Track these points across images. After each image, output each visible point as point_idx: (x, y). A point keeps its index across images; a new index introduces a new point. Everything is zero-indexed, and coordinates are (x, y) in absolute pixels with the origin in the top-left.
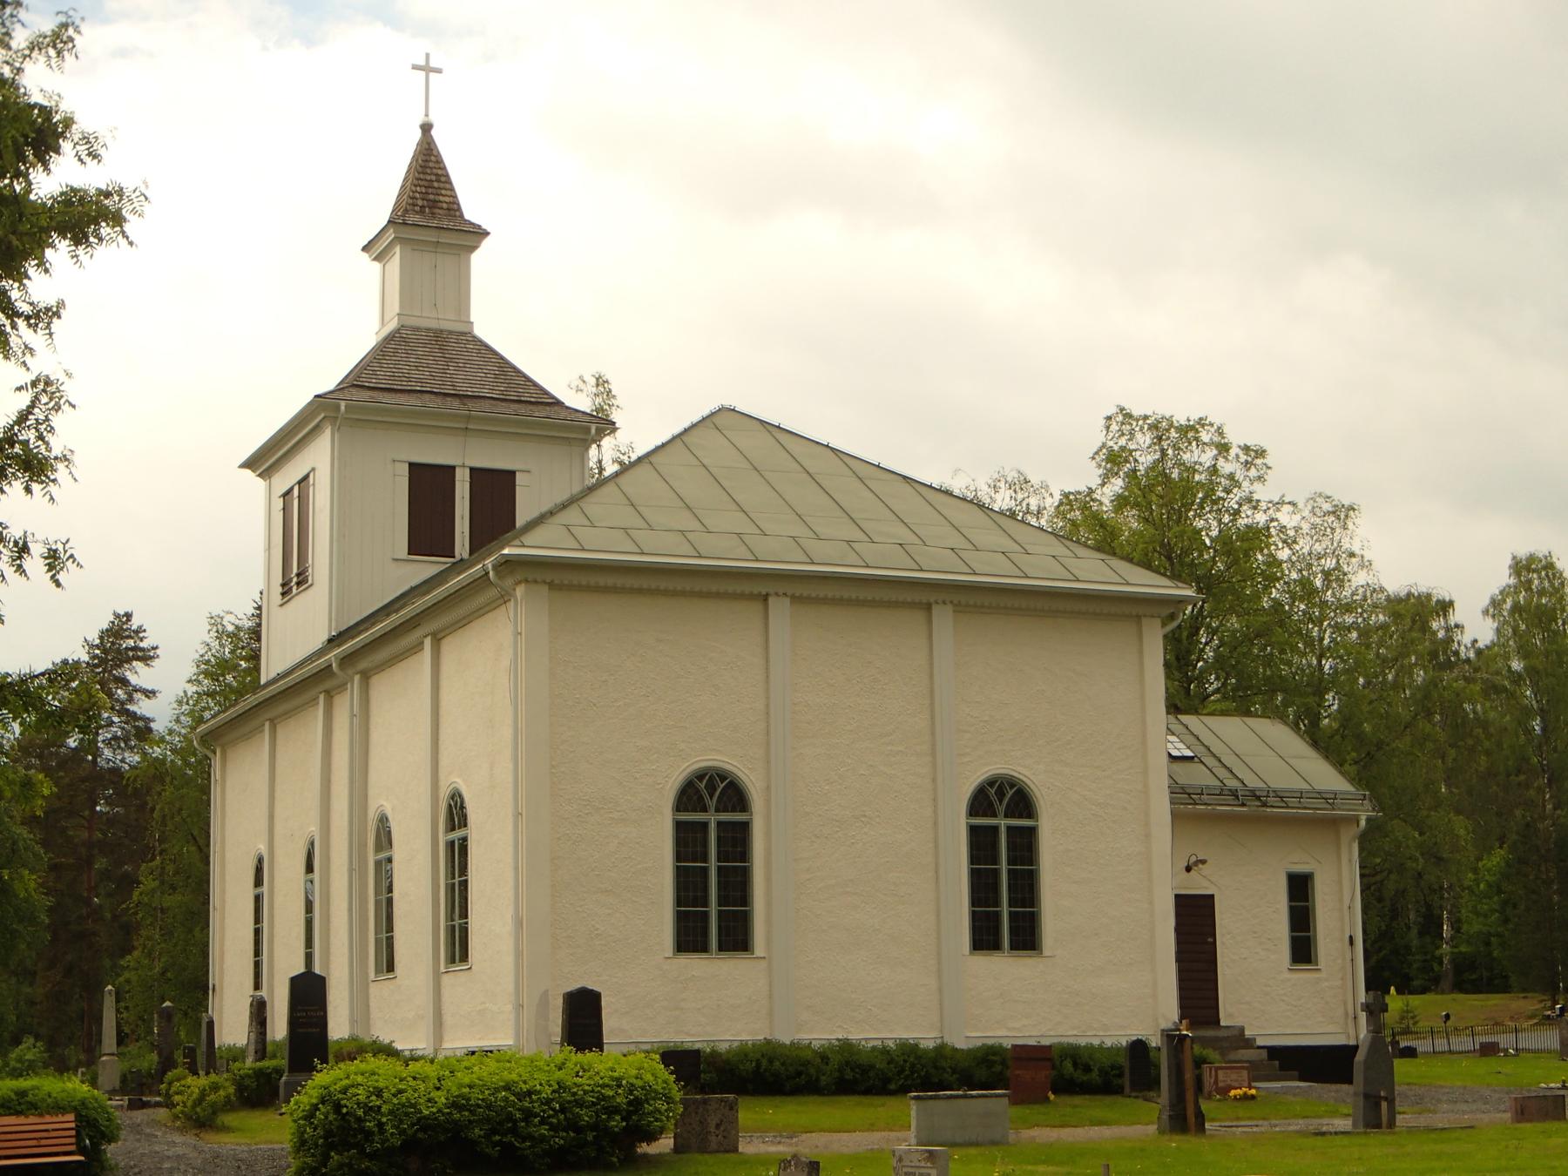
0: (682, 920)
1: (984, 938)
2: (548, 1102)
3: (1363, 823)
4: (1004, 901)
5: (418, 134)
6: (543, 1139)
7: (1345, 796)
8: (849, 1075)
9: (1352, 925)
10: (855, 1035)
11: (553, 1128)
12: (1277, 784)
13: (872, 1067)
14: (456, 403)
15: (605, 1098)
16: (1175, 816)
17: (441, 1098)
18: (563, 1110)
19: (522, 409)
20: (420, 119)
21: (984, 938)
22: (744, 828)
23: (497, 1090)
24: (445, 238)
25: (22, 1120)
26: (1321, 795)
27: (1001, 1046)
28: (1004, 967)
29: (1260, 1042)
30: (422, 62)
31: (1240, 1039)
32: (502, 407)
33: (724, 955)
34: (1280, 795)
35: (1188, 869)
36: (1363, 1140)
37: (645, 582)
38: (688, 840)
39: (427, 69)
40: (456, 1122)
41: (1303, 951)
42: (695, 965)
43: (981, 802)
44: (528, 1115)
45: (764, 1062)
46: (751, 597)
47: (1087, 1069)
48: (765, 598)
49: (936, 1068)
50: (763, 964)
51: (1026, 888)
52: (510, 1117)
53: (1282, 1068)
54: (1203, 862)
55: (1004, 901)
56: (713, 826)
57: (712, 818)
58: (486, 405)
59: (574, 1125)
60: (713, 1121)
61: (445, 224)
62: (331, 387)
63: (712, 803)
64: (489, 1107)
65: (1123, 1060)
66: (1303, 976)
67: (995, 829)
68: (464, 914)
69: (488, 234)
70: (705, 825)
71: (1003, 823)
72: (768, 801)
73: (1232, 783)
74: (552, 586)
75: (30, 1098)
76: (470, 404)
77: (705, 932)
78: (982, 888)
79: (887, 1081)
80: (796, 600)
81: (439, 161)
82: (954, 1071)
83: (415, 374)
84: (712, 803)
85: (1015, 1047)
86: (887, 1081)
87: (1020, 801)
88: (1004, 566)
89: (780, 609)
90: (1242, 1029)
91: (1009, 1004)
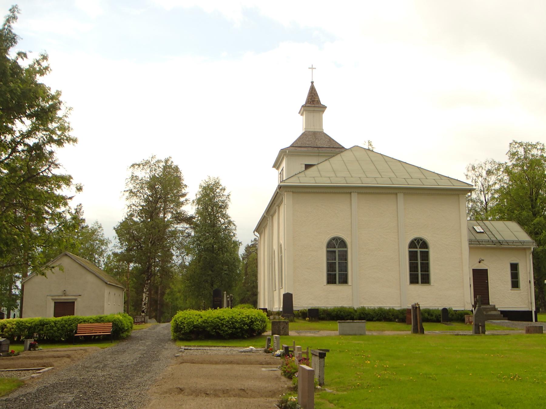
1: (414, 280)
2: (228, 322)
3: (532, 249)
5: (310, 84)
6: (226, 331)
7: (528, 242)
8: (362, 316)
9: (530, 277)
11: (229, 328)
12: (507, 238)
13: (369, 314)
14: (316, 149)
15: (244, 321)
16: (470, 248)
17: (200, 320)
18: (233, 323)
19: (333, 149)
21: (414, 280)
23: (215, 318)
24: (316, 109)
25: (100, 324)
26: (520, 242)
27: (394, 310)
29: (499, 309)
31: (494, 308)
32: (328, 149)
34: (507, 242)
35: (480, 262)
36: (475, 337)
38: (413, 256)
39: (312, 68)
40: (204, 326)
41: (515, 284)
42: (332, 287)
43: (413, 244)
44: (223, 325)
45: (339, 312)
46: (347, 193)
47: (432, 315)
48: (351, 193)
49: (388, 314)
50: (351, 287)
51: (426, 267)
52: (218, 325)
53: (504, 316)
54: (483, 260)
56: (337, 251)
57: (419, 250)
58: (323, 149)
59: (234, 327)
60: (281, 327)
61: (316, 106)
64: (212, 322)
65: (441, 313)
66: (516, 291)
67: (417, 252)
71: (419, 250)
72: (352, 245)
73: (493, 239)
74: (293, 192)
75: (102, 319)
76: (320, 149)
77: (417, 278)
78: (413, 268)
79: (373, 318)
80: (358, 193)
81: (315, 90)
82: (393, 315)
83: (307, 143)
84: (418, 247)
85: (309, 310)
86: (373, 318)
87: (424, 244)
88: (418, 182)
89: (354, 196)
90: (495, 306)
91: (427, 298)
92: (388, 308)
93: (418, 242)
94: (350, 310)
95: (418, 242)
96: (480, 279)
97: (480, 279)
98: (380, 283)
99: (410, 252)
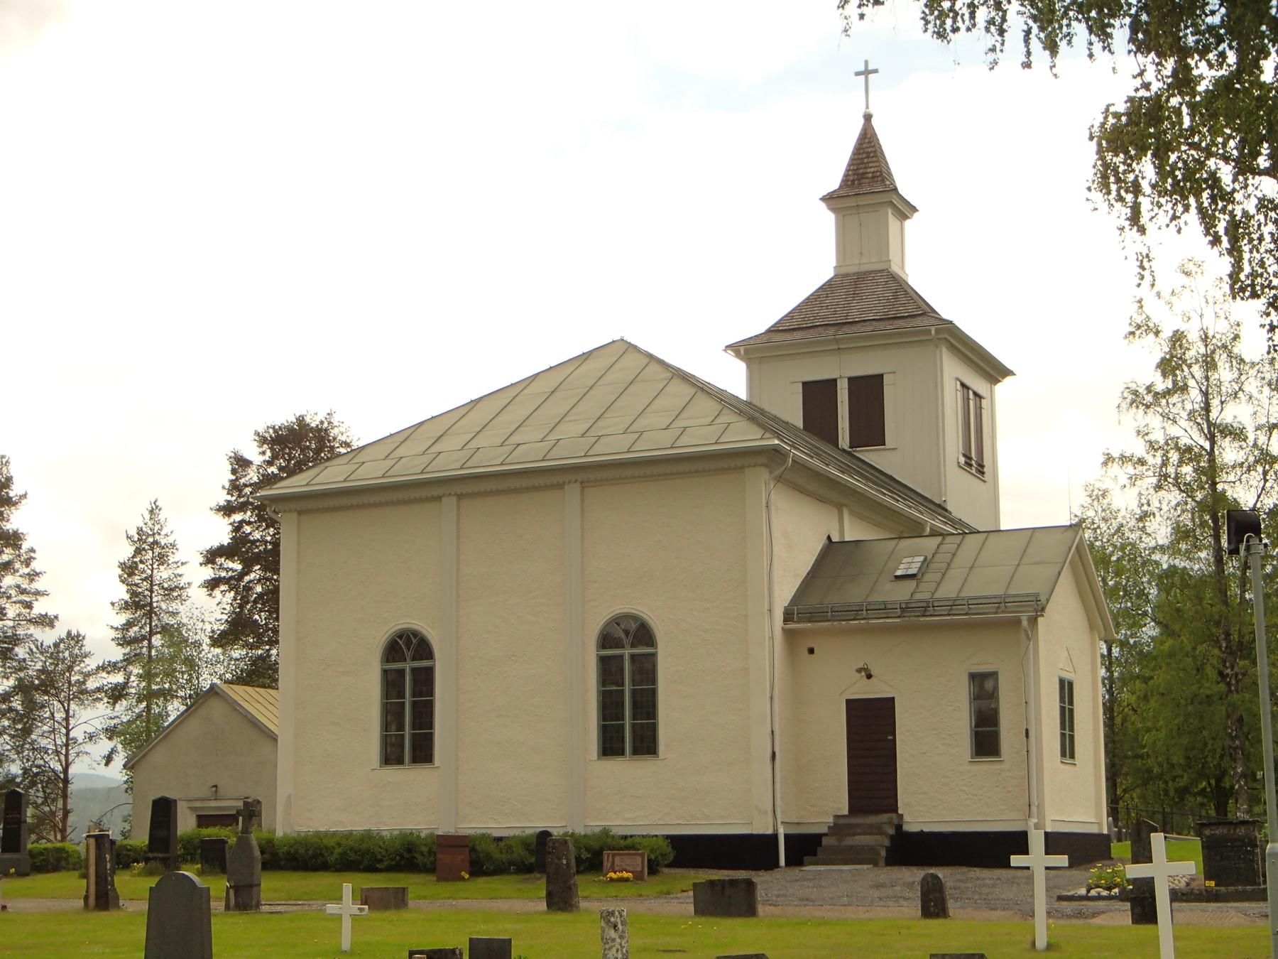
0: (385, 741)
1: (610, 746)
4: (628, 716)
5: (862, 121)
8: (353, 857)
10: (409, 825)
14: (831, 331)
20: (862, 110)
21: (610, 746)
22: (430, 671)
28: (626, 769)
30: (862, 69)
32: (882, 325)
33: (418, 765)
37: (524, 483)
38: (609, 670)
42: (394, 774)
43: (606, 640)
51: (646, 705)
55: (628, 716)
62: (763, 331)
63: (408, 655)
66: (986, 767)
68: (1062, 709)
69: (823, 199)
70: (621, 657)
84: (408, 655)
85: (431, 836)
87: (643, 634)
92: (597, 830)
93: (408, 643)
94: (325, 841)
95: (408, 643)
96: (871, 726)
97: (871, 726)
98: (518, 760)
99: (385, 672)
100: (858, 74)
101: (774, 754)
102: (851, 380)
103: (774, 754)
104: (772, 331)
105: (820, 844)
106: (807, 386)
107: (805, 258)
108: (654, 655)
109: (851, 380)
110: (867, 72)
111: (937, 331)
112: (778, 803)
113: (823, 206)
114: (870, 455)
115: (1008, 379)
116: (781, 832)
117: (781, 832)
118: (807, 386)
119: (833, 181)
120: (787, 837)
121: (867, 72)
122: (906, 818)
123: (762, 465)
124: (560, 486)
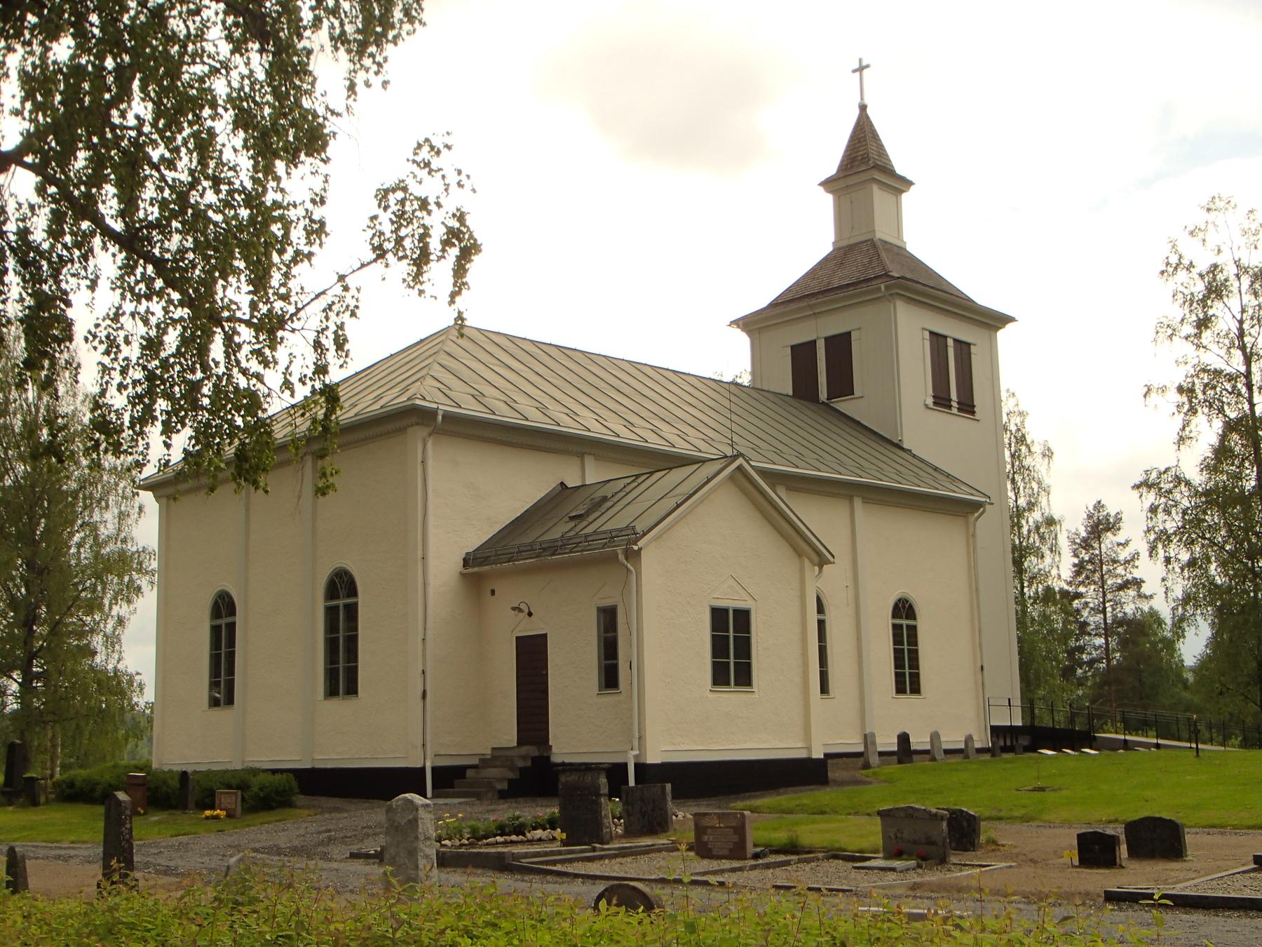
0: (716, 666)
1: (332, 692)
5: (857, 112)
21: (332, 691)
62: (765, 305)
69: (822, 184)
100: (854, 71)
101: (424, 693)
102: (826, 339)
103: (424, 693)
104: (774, 305)
105: (464, 777)
106: (794, 348)
107: (806, 236)
108: (356, 604)
109: (826, 339)
110: (861, 69)
111: (887, 288)
112: (428, 738)
113: (821, 189)
114: (843, 405)
115: (1009, 326)
116: (429, 765)
117: (429, 765)
118: (794, 348)
119: (831, 168)
120: (434, 769)
121: (861, 69)
122: (554, 750)
123: (417, 424)
124: (403, 430)
